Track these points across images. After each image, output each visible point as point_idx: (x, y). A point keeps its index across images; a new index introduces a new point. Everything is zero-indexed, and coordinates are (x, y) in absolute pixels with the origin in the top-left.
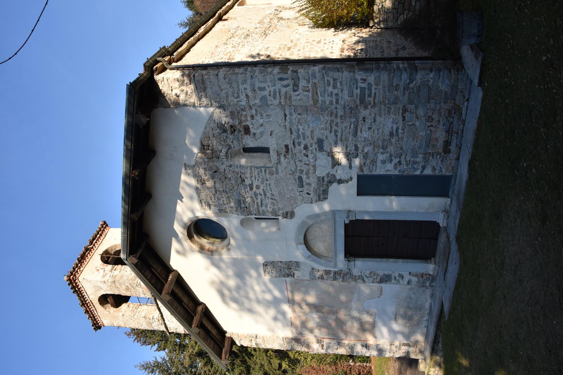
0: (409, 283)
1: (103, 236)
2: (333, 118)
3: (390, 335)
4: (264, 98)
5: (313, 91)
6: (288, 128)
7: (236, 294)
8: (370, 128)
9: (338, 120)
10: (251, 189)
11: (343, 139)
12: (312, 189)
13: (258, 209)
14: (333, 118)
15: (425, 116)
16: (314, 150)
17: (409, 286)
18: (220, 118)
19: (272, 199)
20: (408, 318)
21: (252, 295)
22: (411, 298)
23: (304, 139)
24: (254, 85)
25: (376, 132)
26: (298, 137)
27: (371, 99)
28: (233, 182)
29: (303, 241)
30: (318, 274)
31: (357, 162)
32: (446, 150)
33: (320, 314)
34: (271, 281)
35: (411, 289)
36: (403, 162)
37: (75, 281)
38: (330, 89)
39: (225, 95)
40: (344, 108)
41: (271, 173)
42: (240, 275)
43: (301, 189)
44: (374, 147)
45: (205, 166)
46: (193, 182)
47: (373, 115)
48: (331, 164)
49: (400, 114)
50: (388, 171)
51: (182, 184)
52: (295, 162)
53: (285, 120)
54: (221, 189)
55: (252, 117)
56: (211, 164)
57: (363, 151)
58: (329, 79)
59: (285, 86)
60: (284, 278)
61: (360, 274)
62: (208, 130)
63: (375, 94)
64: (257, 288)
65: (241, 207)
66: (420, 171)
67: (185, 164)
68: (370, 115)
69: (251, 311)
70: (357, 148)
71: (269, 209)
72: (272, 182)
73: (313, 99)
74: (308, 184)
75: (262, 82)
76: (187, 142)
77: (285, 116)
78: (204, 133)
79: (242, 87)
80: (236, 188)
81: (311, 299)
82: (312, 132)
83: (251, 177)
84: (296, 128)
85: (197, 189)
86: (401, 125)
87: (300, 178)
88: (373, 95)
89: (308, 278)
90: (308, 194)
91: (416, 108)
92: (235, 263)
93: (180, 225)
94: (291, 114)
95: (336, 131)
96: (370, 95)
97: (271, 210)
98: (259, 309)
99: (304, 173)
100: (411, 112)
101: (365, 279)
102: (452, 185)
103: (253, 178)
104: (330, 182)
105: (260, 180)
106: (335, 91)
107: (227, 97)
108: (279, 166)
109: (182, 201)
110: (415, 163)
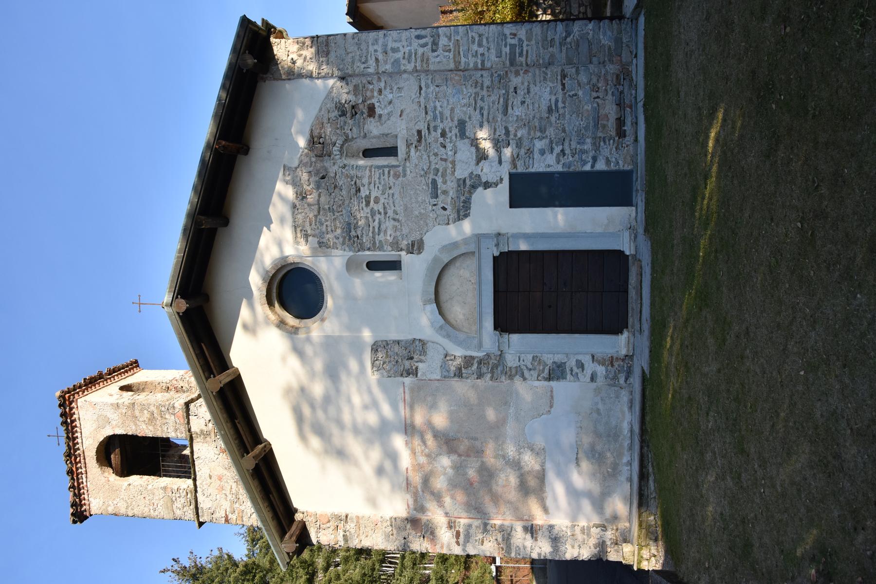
0: (593, 378)
1: (130, 373)
2: (478, 89)
3: (569, 504)
4: (396, 62)
5: (454, 51)
6: (423, 106)
8: (523, 103)
9: (485, 93)
10: (368, 203)
11: (491, 119)
12: (449, 199)
13: (374, 237)
14: (478, 89)
15: (589, 83)
16: (454, 138)
17: (594, 385)
18: (339, 94)
19: (394, 219)
20: (595, 456)
21: (346, 417)
22: (598, 411)
23: (442, 122)
24: (386, 45)
25: (531, 107)
26: (435, 118)
27: (523, 59)
28: (344, 193)
29: (433, 297)
30: (453, 366)
31: (507, 152)
32: (621, 134)
33: (454, 457)
34: (380, 383)
35: (597, 391)
36: (567, 151)
37: (71, 403)
38: (475, 47)
39: (350, 60)
40: (492, 76)
41: (397, 176)
42: (333, 372)
43: (434, 201)
44: (529, 129)
45: (311, 169)
46: (289, 192)
47: (526, 84)
48: (474, 158)
49: (559, 81)
50: (549, 166)
51: (275, 198)
52: (429, 156)
53: (420, 93)
54: (327, 207)
55: (380, 91)
56: (319, 165)
57: (515, 135)
58: (474, 34)
59: (424, 45)
60: (401, 379)
61: (517, 364)
62: (322, 113)
63: (527, 52)
64: (357, 400)
65: (351, 237)
66: (589, 164)
67: (284, 167)
68: (523, 83)
69: (341, 454)
70: (507, 133)
71: (388, 238)
72: (396, 190)
73: (455, 61)
74: (445, 192)
75: (395, 41)
76: (293, 130)
77: (421, 88)
78: (317, 118)
79: (371, 49)
80: (347, 202)
81: (440, 420)
82: (452, 110)
83: (370, 183)
84: (432, 104)
85: (294, 206)
86: (560, 97)
87: (434, 182)
88: (525, 53)
89: (439, 377)
90: (444, 209)
92: (330, 344)
93: (258, 271)
94: (427, 87)
95: (481, 108)
96: (521, 55)
97: (390, 239)
98: (355, 446)
99: (440, 174)
100: (572, 79)
102: (634, 179)
103: (372, 185)
104: (474, 187)
105: (381, 188)
106: (481, 50)
107: (353, 62)
108: (408, 164)
109: (269, 229)
110: (583, 152)
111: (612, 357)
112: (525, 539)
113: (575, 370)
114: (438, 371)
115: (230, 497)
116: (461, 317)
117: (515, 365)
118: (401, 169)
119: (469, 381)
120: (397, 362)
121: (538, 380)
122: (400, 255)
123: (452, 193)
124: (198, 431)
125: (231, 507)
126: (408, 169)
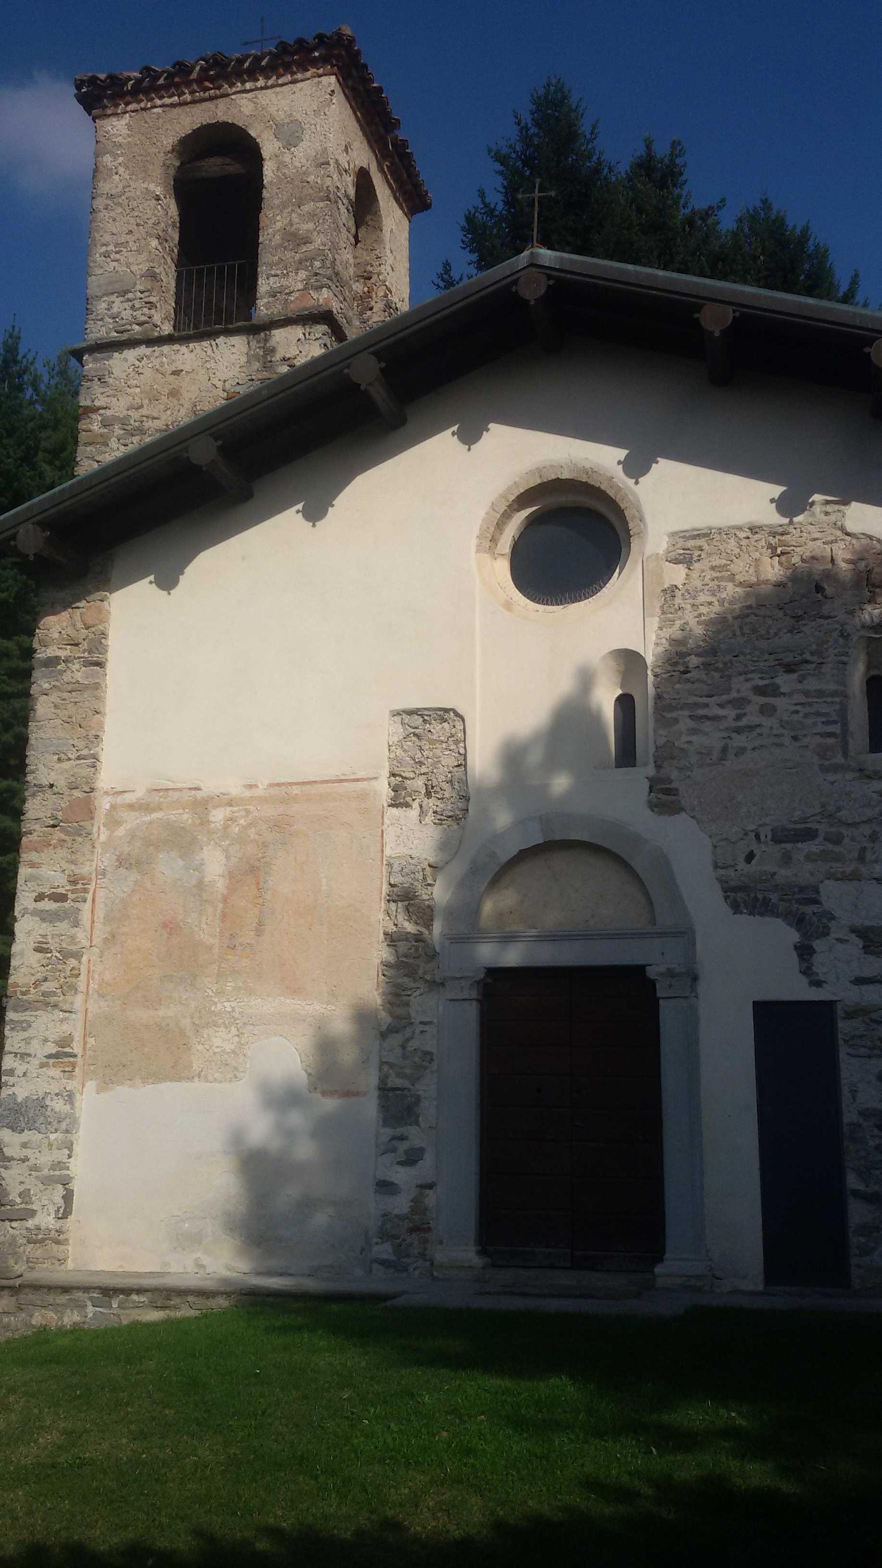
10: (760, 691)
12: (770, 868)
13: (685, 706)
19: (725, 749)
48: (867, 923)
50: (854, 1092)
52: (869, 821)
66: (861, 1187)
74: (787, 859)
83: (807, 694)
87: (809, 835)
90: (750, 858)
99: (830, 846)
103: (803, 699)
104: (799, 922)
105: (795, 717)
108: (849, 776)
111: (429, 1229)
112: (46, 1040)
113: (403, 1146)
114: (403, 850)
115: (135, 415)
116: (79, 1318)
117: (413, 1014)
118: (839, 759)
119: (381, 916)
120: (421, 763)
121: (382, 1063)
122: (645, 764)
123: (784, 874)
124: (272, 343)
125: (115, 418)
126: (838, 776)
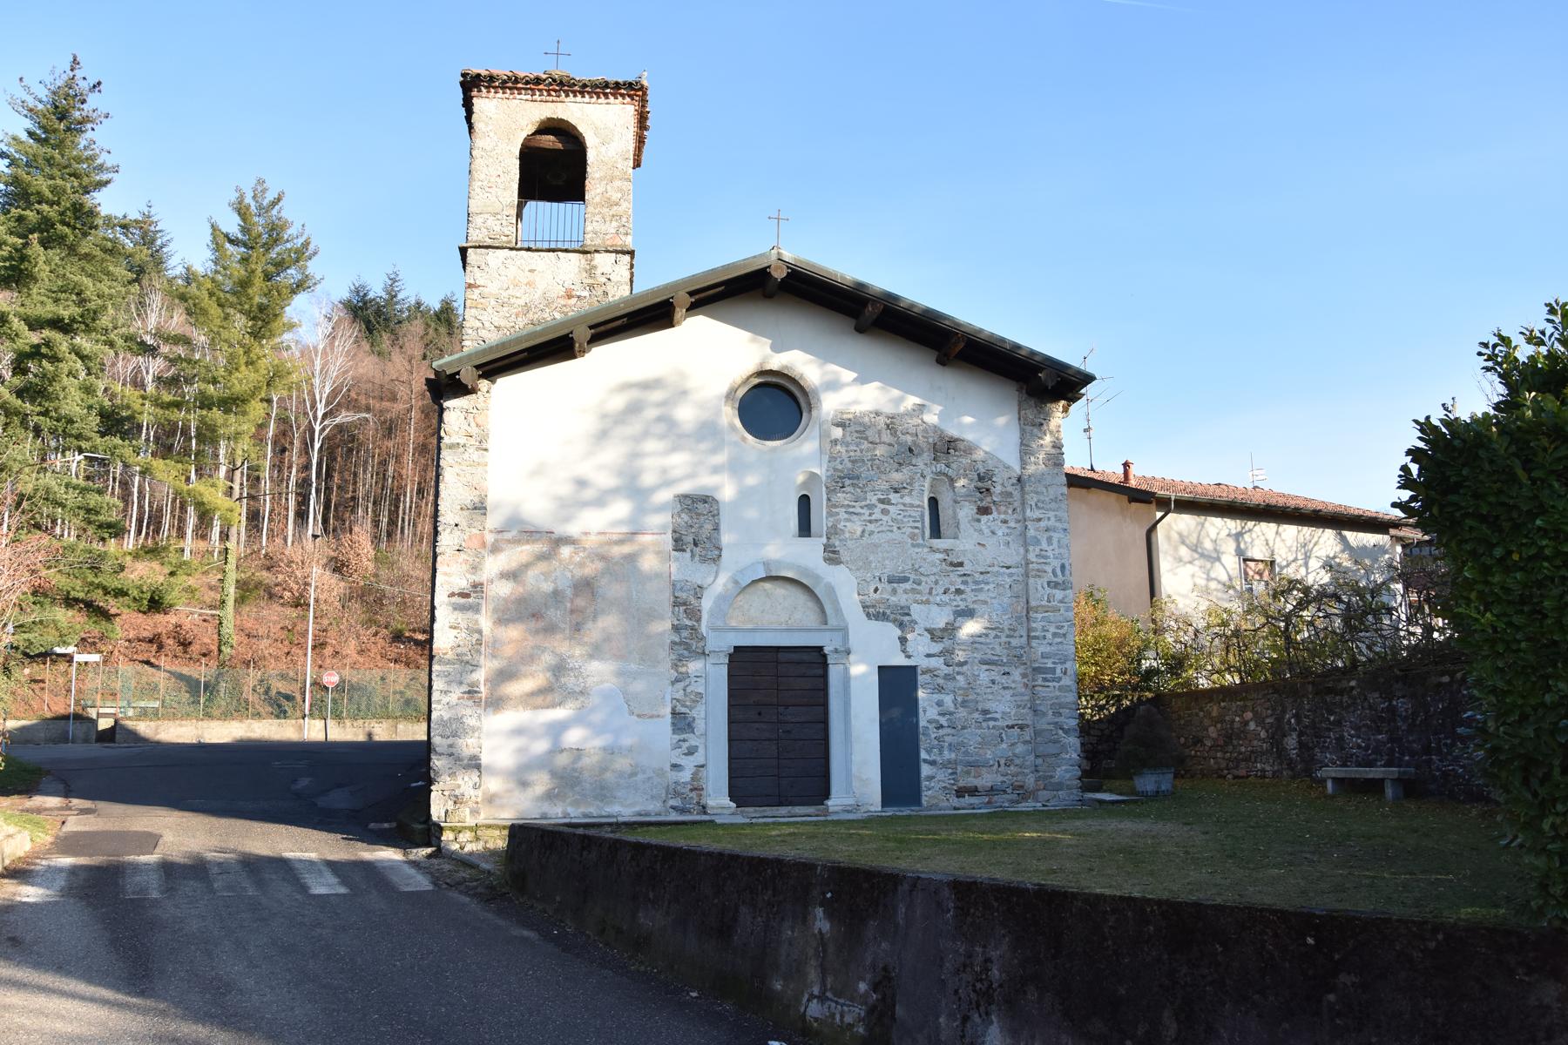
7: (651, 413)
8: (993, 682)
9: (1004, 639)
10: (882, 501)
17: (668, 767)
27: (1040, 682)
35: (660, 773)
38: (1052, 629)
43: (884, 578)
55: (1005, 522)
59: (1054, 572)
69: (602, 436)
74: (894, 591)
79: (1051, 514)
82: (985, 603)
87: (906, 580)
91: (1025, 742)
94: (1010, 575)
96: (1045, 680)
101: (680, 685)
104: (901, 625)
106: (1049, 636)
